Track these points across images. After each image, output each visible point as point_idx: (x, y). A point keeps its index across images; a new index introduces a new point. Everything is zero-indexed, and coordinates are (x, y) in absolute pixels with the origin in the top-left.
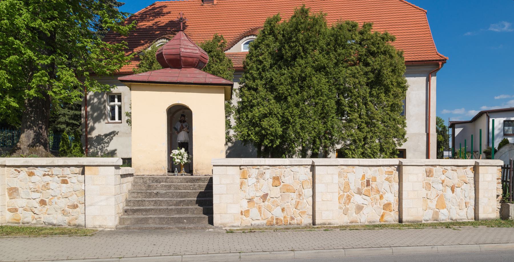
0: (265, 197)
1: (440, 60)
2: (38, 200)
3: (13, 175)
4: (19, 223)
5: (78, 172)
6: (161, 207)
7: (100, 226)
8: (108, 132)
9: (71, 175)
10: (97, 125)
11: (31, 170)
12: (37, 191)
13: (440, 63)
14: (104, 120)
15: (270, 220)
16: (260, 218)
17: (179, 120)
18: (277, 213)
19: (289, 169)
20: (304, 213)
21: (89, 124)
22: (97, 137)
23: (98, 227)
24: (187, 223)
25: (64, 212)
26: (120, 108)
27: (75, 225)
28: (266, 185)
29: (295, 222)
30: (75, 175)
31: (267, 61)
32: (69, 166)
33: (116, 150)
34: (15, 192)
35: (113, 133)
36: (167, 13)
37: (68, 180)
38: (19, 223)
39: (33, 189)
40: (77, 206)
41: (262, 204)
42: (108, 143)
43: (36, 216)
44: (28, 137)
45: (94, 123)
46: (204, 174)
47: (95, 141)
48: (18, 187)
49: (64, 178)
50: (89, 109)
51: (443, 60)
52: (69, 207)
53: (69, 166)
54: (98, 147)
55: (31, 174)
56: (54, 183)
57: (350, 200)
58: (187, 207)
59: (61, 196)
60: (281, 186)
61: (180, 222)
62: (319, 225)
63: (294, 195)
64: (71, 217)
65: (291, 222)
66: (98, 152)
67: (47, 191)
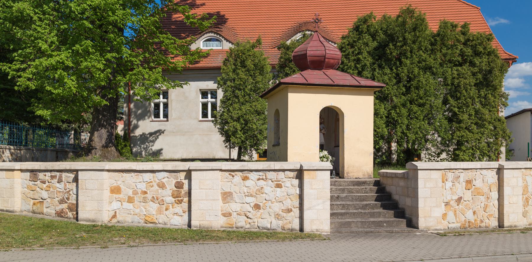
0: (459, 200)
1: (510, 59)
2: (252, 205)
3: (226, 180)
4: (233, 228)
5: (292, 176)
6: (348, 211)
7: (317, 230)
8: (153, 131)
9: (285, 180)
10: (141, 123)
11: (246, 174)
12: (252, 196)
13: (511, 62)
14: (149, 118)
15: (464, 223)
16: (455, 221)
17: (331, 123)
18: (470, 216)
19: (479, 171)
20: (491, 215)
21: (132, 121)
22: (141, 135)
23: (315, 231)
24: (387, 227)
25: (278, 217)
26: (166, 105)
27: (289, 229)
28: (460, 189)
29: (483, 225)
30: (290, 179)
31: (368, 60)
32: (284, 171)
33: (162, 149)
34: (229, 196)
35: (159, 132)
36: (201, 5)
37: (283, 184)
38: (233, 228)
39: (247, 194)
40: (291, 210)
41: (457, 207)
42: (153, 142)
43: (249, 220)
44: (100, 137)
45: (138, 121)
46: (354, 177)
47: (139, 140)
48: (232, 191)
49: (278, 183)
50: (132, 106)
51: (513, 59)
52: (283, 211)
53: (284, 171)
54: (142, 146)
55: (245, 179)
56: (268, 188)
57: (528, 202)
58: (372, 211)
59: (275, 200)
60: (472, 189)
61: (380, 226)
62: (506, 227)
63: (482, 198)
64: (285, 221)
65: (481, 225)
66: (142, 151)
67: (261, 195)
